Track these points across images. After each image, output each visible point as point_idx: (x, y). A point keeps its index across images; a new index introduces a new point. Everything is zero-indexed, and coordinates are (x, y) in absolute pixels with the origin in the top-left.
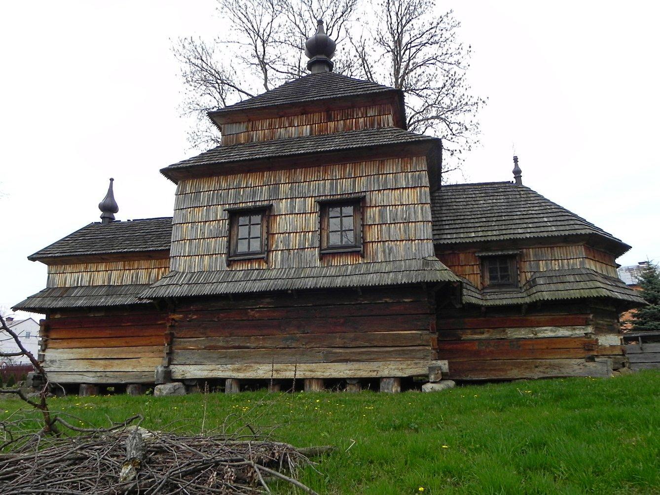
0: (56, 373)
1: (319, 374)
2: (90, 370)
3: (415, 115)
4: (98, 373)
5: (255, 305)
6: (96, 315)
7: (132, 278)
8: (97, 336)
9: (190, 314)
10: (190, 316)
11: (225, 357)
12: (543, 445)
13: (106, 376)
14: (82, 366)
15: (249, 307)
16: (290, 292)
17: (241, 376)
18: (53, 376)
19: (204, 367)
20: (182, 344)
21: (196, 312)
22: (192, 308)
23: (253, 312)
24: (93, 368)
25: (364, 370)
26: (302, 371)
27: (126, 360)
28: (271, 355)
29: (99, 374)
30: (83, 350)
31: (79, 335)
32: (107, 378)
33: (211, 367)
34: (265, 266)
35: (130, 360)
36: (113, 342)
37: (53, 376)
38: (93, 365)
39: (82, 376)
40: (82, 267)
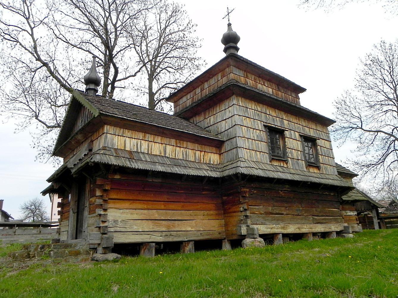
0: (122, 233)
1: (314, 230)
2: (156, 230)
3: (142, 33)
4: (164, 232)
5: (282, 188)
6: (154, 181)
7: (183, 154)
8: (157, 200)
9: (253, 189)
10: (253, 191)
11: (274, 220)
12: (106, 290)
13: (171, 235)
14: (147, 226)
15: (280, 189)
16: (309, 183)
17: (285, 232)
18: (119, 236)
19: (268, 226)
20: (252, 209)
21: (255, 188)
22: (252, 185)
23: (282, 193)
24: (158, 228)
25: (320, 228)
26: (305, 229)
27: (184, 221)
28: (296, 217)
29: (164, 234)
30: (146, 211)
31: (140, 198)
32: (172, 237)
33: (271, 226)
34: (285, 166)
35: (187, 221)
36: (172, 206)
37: (119, 236)
38: (158, 226)
39: (150, 236)
40: (141, 135)
